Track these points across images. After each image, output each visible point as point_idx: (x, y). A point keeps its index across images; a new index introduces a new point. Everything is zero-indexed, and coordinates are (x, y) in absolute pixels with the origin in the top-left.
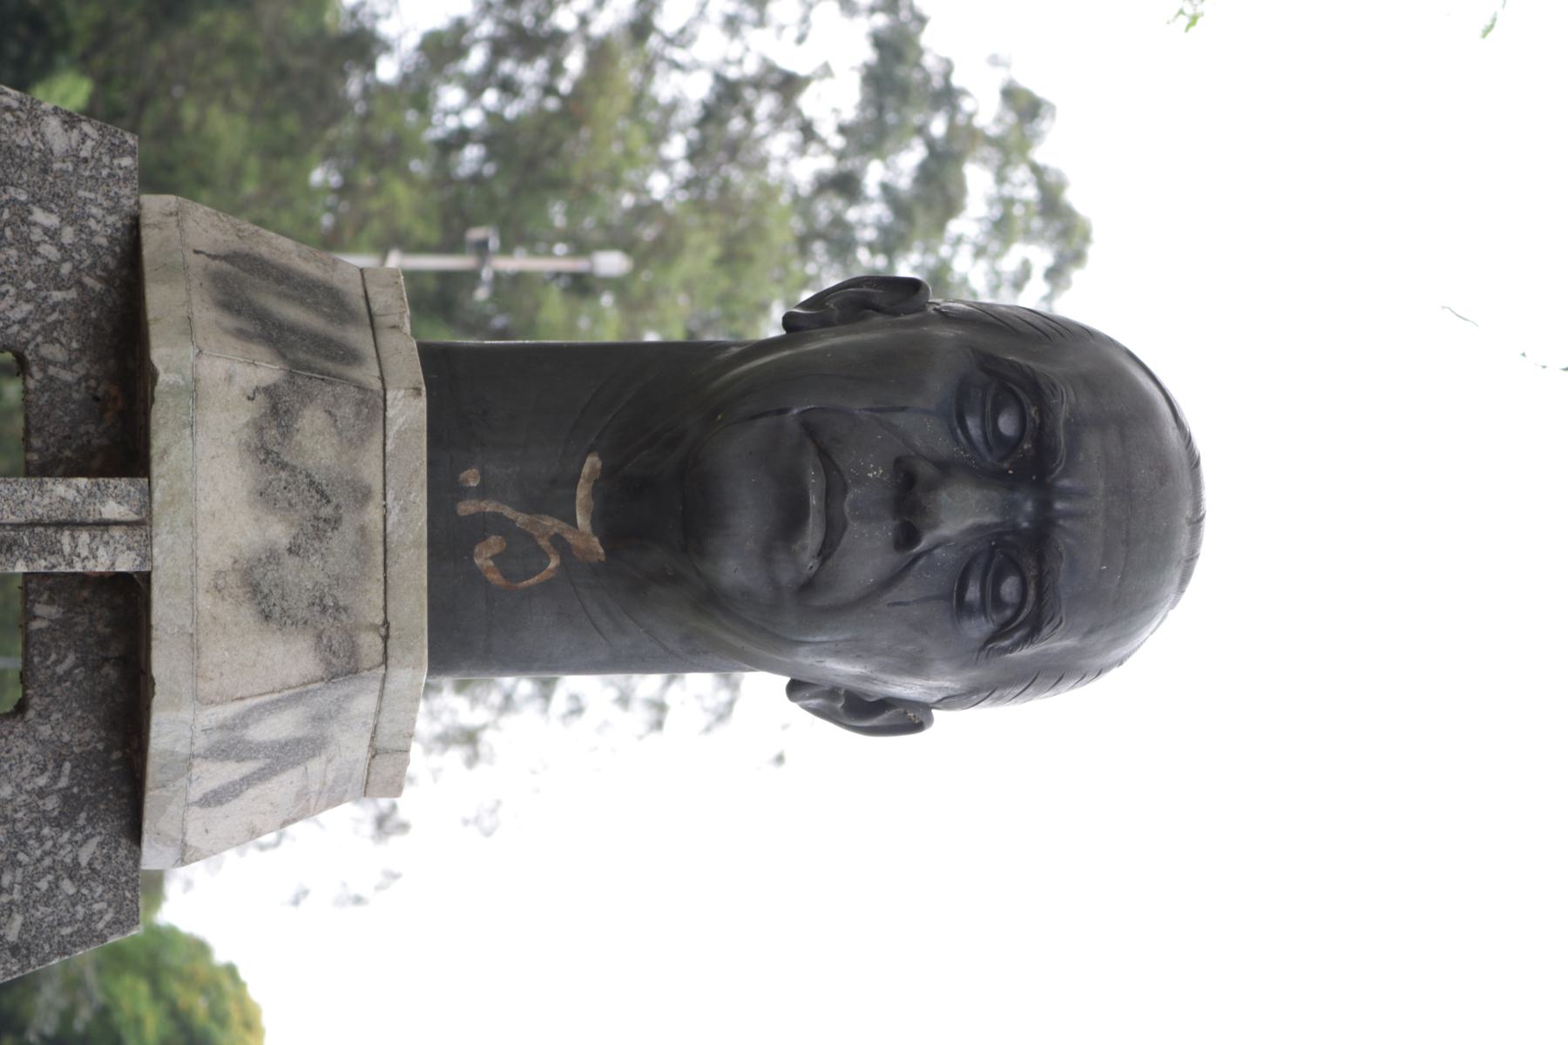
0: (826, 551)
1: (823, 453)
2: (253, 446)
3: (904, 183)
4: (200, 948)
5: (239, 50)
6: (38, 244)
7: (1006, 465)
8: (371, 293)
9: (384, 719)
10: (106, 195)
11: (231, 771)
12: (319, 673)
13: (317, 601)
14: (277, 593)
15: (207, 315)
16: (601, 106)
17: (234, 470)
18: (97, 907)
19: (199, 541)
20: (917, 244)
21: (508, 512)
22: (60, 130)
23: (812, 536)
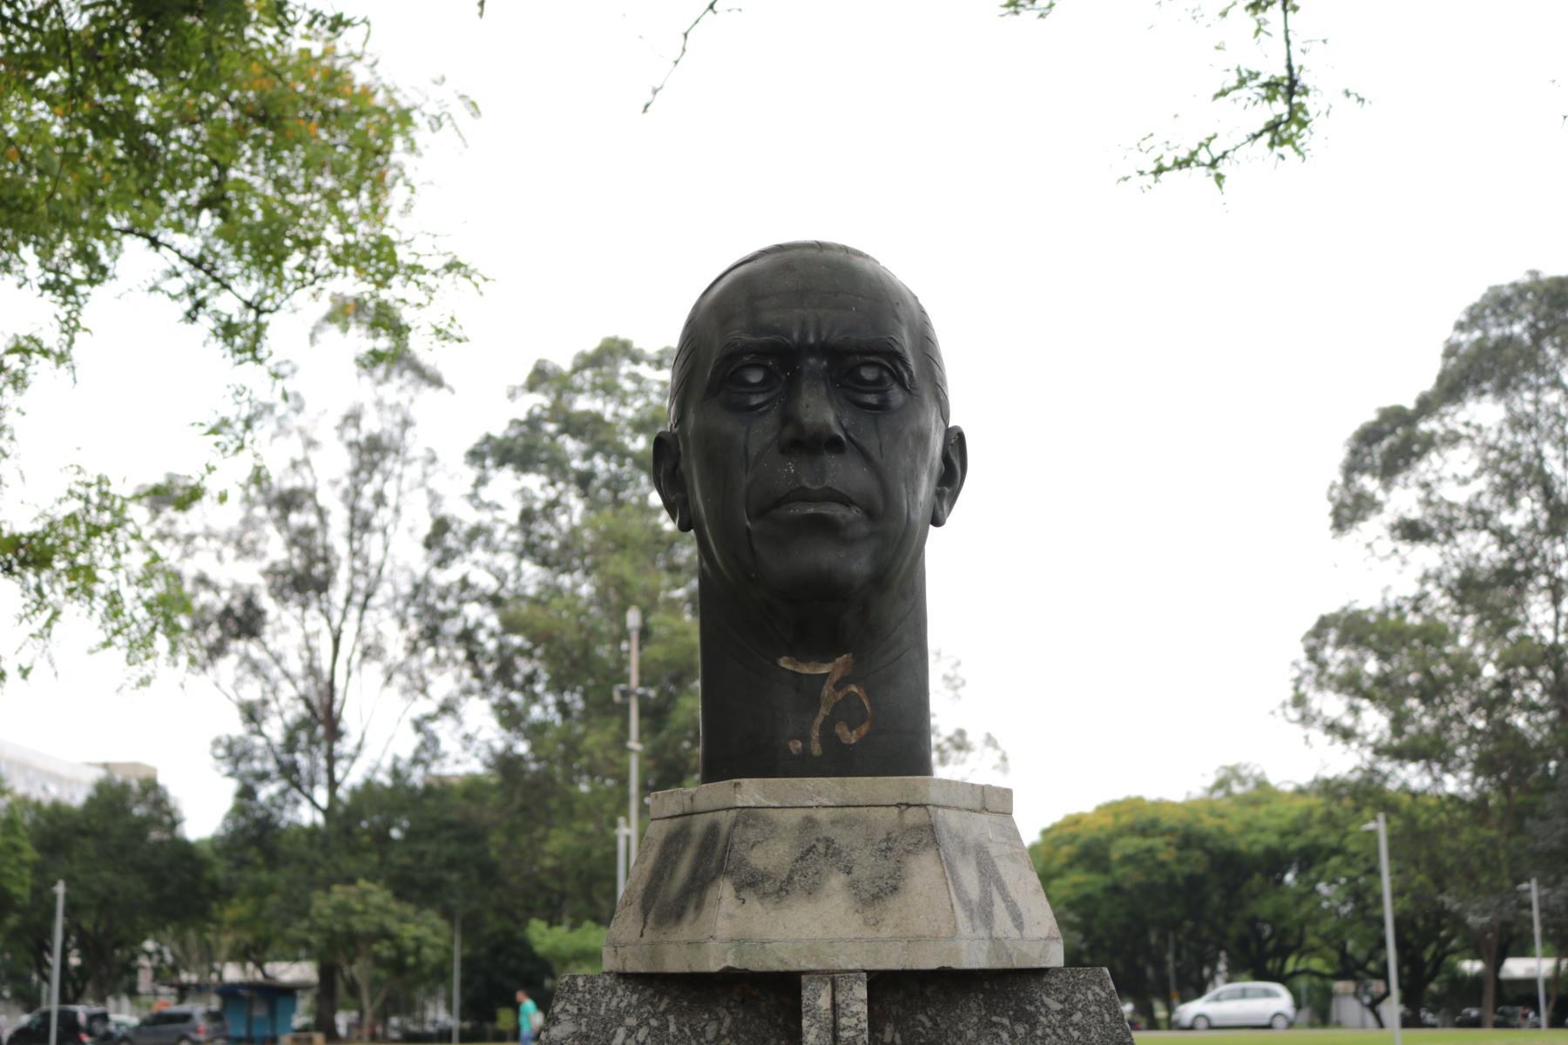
0: (846, 501)
1: (778, 503)
3: (584, 447)
5: (512, 833)
7: (783, 377)
9: (962, 804)
10: (603, 995)
11: (1000, 910)
12: (933, 852)
14: (879, 882)
15: (685, 931)
16: (540, 624)
18: (1091, 997)
20: (619, 438)
21: (819, 720)
22: (559, 1027)
23: (836, 511)
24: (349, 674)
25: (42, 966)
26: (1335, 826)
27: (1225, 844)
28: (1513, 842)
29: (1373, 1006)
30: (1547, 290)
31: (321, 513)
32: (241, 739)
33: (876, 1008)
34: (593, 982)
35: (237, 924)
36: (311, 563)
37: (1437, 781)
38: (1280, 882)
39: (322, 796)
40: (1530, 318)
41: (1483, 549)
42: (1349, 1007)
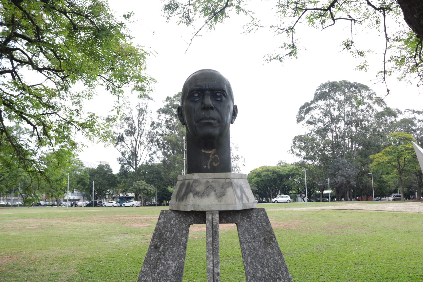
0: (214, 119)
1: (201, 120)
9: (237, 178)
11: (244, 198)
14: (221, 193)
15: (184, 203)
21: (209, 162)
23: (212, 121)
24: (138, 147)
25: (91, 194)
26: (297, 170)
27: (280, 173)
29: (303, 199)
31: (133, 121)
33: (221, 216)
35: (122, 187)
36: (132, 129)
39: (134, 167)
41: (321, 125)
42: (299, 199)
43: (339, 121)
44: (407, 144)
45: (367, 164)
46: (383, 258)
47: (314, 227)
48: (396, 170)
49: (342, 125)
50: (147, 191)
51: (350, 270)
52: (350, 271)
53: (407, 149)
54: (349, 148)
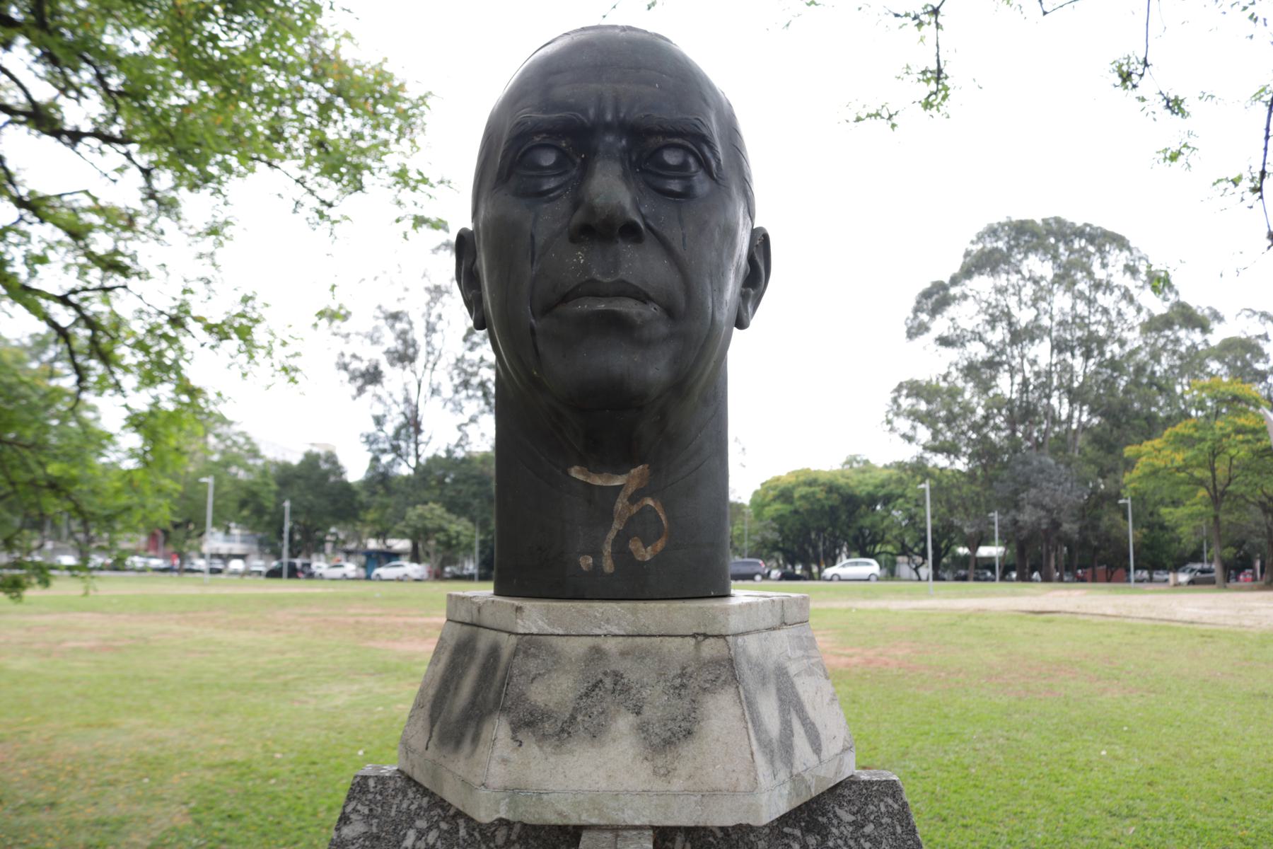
0: (642, 297)
1: (565, 299)
2: (557, 743)
4: (756, 493)
6: (427, 844)
8: (460, 620)
9: (762, 625)
10: (394, 797)
12: (733, 690)
13: (677, 691)
14: (671, 725)
17: (575, 758)
18: (883, 809)
19: (629, 789)
21: (611, 535)
23: (628, 307)
25: (281, 538)
27: (849, 491)
28: (987, 493)
30: (1015, 226)
31: (410, 323)
32: (374, 434)
34: (384, 784)
35: (374, 522)
37: (952, 463)
38: (874, 510)
40: (1006, 239)
41: (978, 351)
42: (904, 569)
43: (1032, 340)
44: (1239, 416)
45: (1113, 470)
46: (1198, 795)
47: (960, 671)
48: (1202, 492)
49: (1041, 352)
50: (448, 535)
51: (1096, 838)
52: (1096, 842)
53: (1239, 430)
54: (1060, 423)
